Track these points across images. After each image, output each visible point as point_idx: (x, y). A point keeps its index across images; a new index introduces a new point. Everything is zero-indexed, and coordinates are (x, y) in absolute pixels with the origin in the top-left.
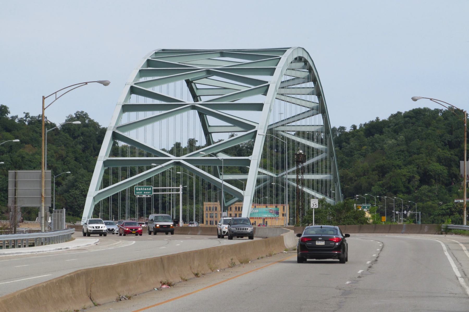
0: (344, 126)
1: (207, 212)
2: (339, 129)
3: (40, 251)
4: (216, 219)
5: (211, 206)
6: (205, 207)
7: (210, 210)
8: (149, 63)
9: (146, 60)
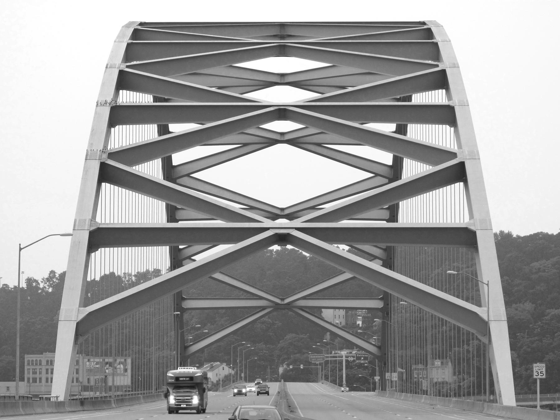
1: (29, 367)
2: (153, 272)
5: (34, 359)
6: (26, 360)
7: (33, 364)
8: (136, 34)
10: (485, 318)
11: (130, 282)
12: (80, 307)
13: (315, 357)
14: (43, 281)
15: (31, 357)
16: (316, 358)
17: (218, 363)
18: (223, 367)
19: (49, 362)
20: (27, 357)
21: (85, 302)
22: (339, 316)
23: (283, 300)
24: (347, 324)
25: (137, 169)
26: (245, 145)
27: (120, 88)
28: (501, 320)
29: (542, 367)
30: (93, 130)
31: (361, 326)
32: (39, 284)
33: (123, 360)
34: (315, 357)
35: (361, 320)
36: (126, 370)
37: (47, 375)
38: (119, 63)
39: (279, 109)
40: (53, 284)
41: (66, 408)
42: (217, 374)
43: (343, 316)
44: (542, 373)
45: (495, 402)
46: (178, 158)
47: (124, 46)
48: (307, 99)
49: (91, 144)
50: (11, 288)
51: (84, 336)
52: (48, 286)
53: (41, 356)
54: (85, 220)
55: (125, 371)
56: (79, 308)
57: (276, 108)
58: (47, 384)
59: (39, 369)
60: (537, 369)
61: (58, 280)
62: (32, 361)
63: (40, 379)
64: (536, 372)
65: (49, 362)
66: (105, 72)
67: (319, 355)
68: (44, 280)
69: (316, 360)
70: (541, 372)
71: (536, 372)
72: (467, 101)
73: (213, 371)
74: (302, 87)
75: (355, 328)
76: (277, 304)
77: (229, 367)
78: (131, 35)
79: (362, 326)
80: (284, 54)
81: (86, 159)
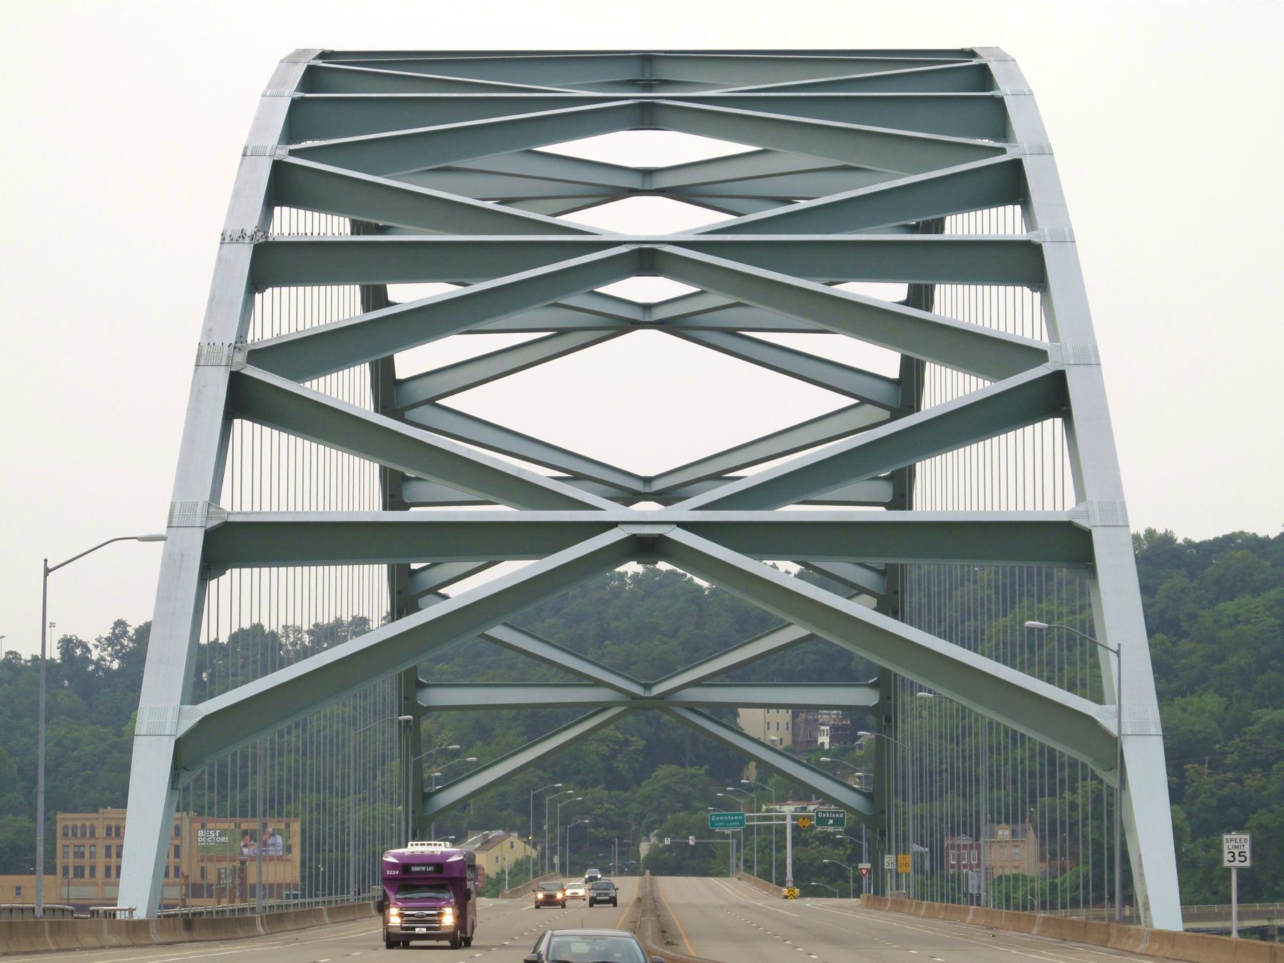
1: (66, 842)
4: (177, 860)
5: (88, 824)
6: (59, 826)
7: (75, 834)
8: (312, 78)
9: (299, 71)
10: (1111, 726)
11: (298, 647)
12: (182, 703)
13: (722, 818)
14: (98, 643)
15: (90, 819)
16: (724, 821)
17: (500, 832)
18: (512, 843)
19: (113, 829)
20: (62, 819)
21: (196, 691)
22: (778, 724)
23: (648, 687)
24: (794, 742)
25: (315, 388)
26: (561, 332)
29: (1243, 841)
31: (827, 746)
32: (89, 650)
33: (282, 826)
34: (722, 818)
35: (827, 735)
36: (288, 849)
37: (66, 860)
38: (272, 145)
39: (640, 250)
40: (120, 651)
42: (497, 858)
43: (787, 724)
44: (1243, 856)
46: (408, 363)
48: (704, 227)
49: (208, 331)
50: (26, 662)
52: (110, 655)
53: (94, 815)
54: (196, 504)
55: (286, 851)
56: (182, 706)
57: (634, 248)
58: (108, 880)
60: (1230, 847)
62: (75, 827)
63: (93, 869)
65: (113, 829)
66: (241, 164)
67: (731, 815)
68: (100, 642)
69: (725, 825)
70: (1241, 854)
72: (1071, 231)
74: (690, 198)
76: (635, 697)
77: (525, 842)
79: (830, 749)
80: (652, 124)
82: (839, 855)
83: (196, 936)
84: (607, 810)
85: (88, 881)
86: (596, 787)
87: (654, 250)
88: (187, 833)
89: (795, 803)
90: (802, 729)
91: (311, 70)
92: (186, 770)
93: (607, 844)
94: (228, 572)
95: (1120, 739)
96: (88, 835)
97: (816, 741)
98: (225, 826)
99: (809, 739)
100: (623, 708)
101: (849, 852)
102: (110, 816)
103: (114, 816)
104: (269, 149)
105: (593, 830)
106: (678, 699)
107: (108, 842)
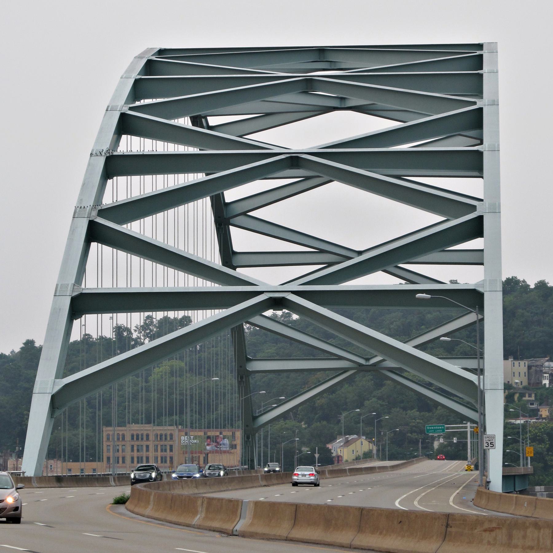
0: (530, 285)
1: (108, 443)
3: (240, 514)
4: (171, 453)
5: (121, 433)
7: (138, 439)
9: (144, 61)
12: (55, 379)
13: (432, 428)
14: (136, 329)
15: (122, 430)
17: (355, 436)
18: (362, 442)
20: (106, 431)
21: (62, 372)
22: (519, 373)
23: (367, 360)
24: (529, 384)
26: (307, 178)
27: (123, 132)
28: (498, 389)
29: (492, 437)
30: (84, 185)
31: (547, 386)
34: (432, 428)
35: (548, 379)
36: (233, 446)
39: (291, 157)
40: (149, 333)
41: (33, 484)
42: (353, 451)
43: (525, 373)
44: (492, 444)
45: (140, 462)
47: (132, 82)
48: (321, 145)
49: (80, 200)
51: (61, 409)
53: (123, 428)
54: (68, 285)
55: (231, 448)
56: (55, 380)
57: (288, 156)
58: (133, 465)
59: (122, 446)
60: (487, 440)
61: (157, 328)
63: (124, 458)
64: (486, 443)
65: (135, 437)
67: (437, 426)
69: (434, 432)
70: (492, 443)
71: (486, 443)
72: (499, 145)
73: (348, 446)
74: (367, 112)
75: (540, 389)
76: (360, 365)
77: (369, 442)
78: (143, 66)
79: (549, 387)
80: (312, 89)
81: (74, 217)
82: (541, 448)
83: (63, 485)
84: (418, 423)
85: (121, 465)
86: (413, 410)
87: (298, 157)
88: (177, 438)
89: (523, 419)
90: (534, 376)
91: (149, 63)
92: (58, 409)
93: (416, 442)
94: (84, 316)
95: (484, 391)
96: (121, 439)
97: (541, 383)
98: (196, 434)
99: (537, 382)
100: (355, 371)
101: (548, 446)
102: (133, 428)
103: (136, 428)
104: (119, 107)
105: (410, 435)
106: (383, 366)
107: (156, 443)
